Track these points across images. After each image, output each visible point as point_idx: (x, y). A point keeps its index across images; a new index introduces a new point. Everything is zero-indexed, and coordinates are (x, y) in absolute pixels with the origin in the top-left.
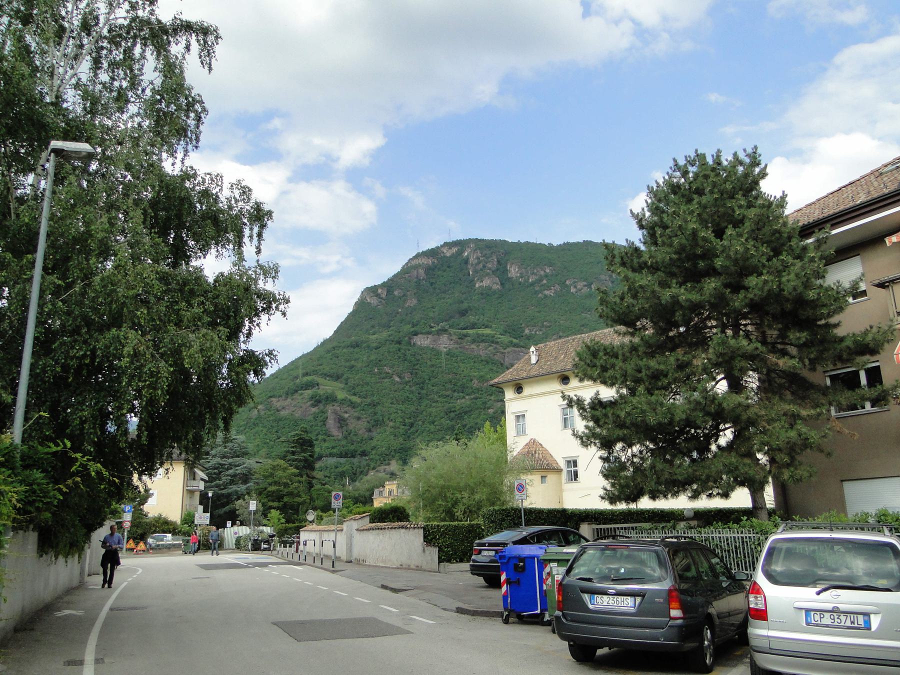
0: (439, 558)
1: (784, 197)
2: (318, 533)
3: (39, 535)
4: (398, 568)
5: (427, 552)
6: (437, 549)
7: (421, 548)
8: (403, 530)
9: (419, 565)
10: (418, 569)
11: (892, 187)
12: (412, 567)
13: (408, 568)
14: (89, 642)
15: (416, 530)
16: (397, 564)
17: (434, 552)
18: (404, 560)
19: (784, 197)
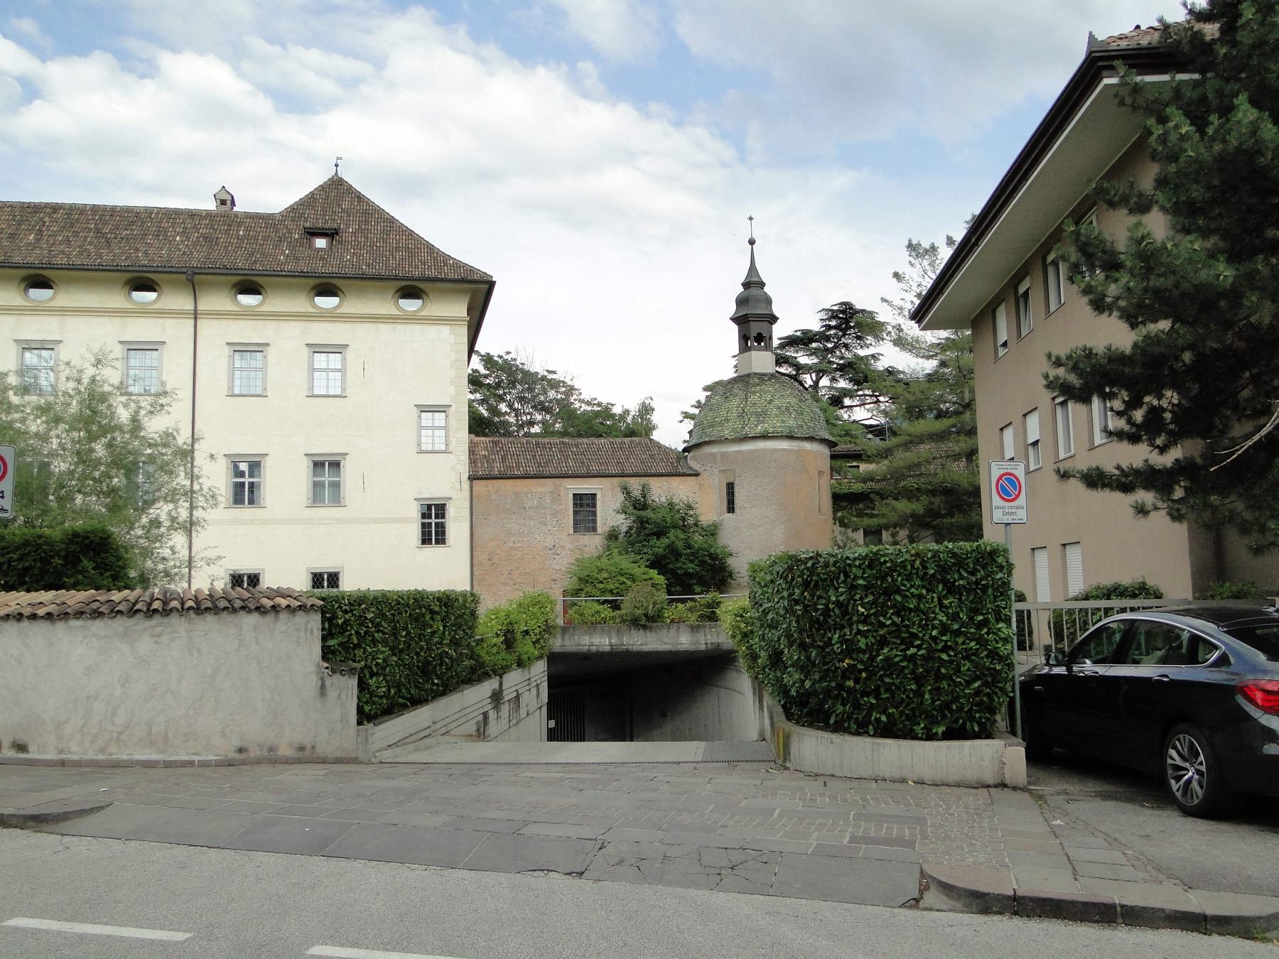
0: (360, 710)
1: (646, 410)
2: (316, 392)
3: (209, 215)
4: (231, 764)
5: (332, 694)
6: (353, 682)
7: (314, 681)
8: (252, 619)
9: (307, 742)
10: (306, 756)
11: (1276, 689)
12: (285, 751)
13: (272, 759)
14: (1048, 588)
15: (301, 618)
16: (223, 748)
17: (346, 689)
18: (254, 730)
19: (646, 410)
